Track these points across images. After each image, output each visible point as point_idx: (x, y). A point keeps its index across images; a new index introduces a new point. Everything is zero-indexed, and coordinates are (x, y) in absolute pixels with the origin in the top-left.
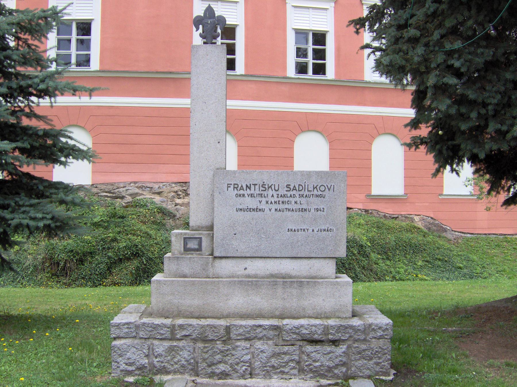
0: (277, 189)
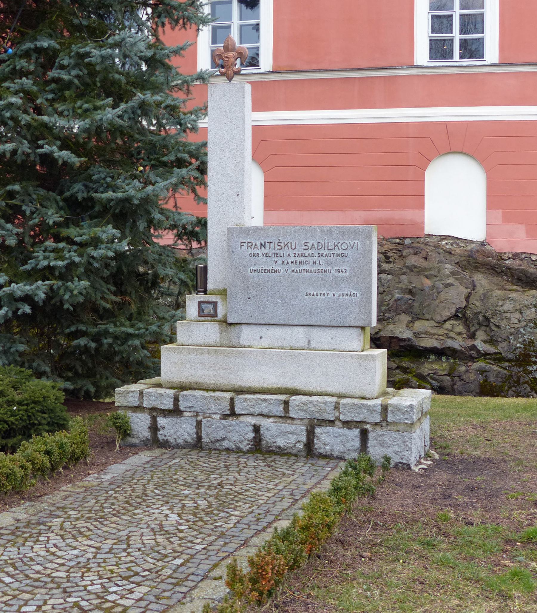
0: (293, 247)
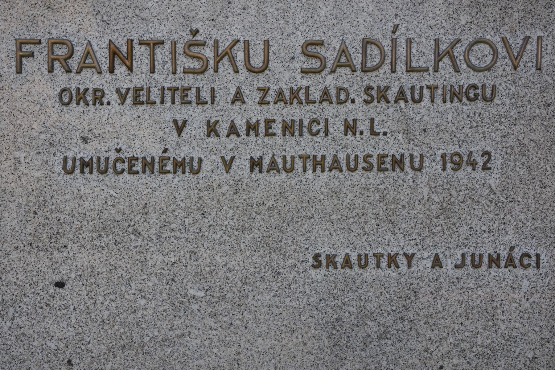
0: (257, 62)
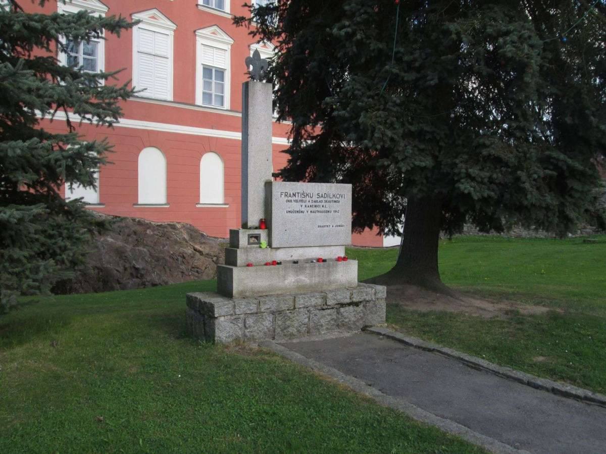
0: (311, 196)
